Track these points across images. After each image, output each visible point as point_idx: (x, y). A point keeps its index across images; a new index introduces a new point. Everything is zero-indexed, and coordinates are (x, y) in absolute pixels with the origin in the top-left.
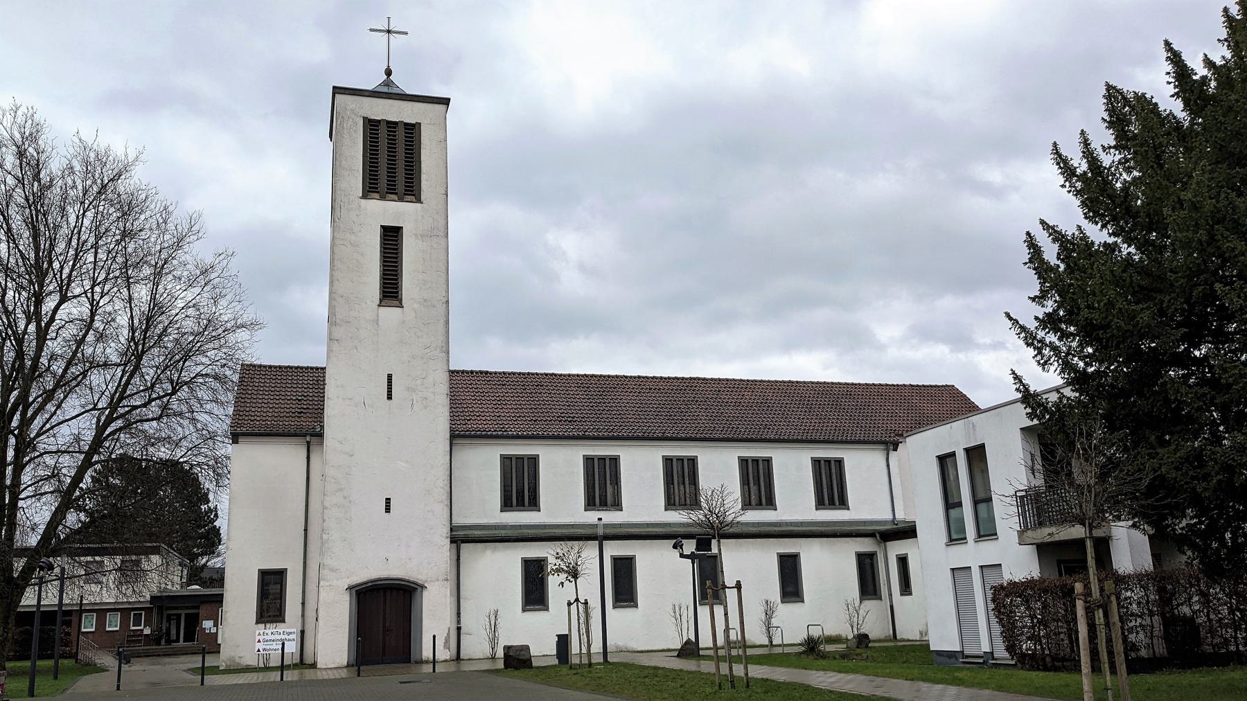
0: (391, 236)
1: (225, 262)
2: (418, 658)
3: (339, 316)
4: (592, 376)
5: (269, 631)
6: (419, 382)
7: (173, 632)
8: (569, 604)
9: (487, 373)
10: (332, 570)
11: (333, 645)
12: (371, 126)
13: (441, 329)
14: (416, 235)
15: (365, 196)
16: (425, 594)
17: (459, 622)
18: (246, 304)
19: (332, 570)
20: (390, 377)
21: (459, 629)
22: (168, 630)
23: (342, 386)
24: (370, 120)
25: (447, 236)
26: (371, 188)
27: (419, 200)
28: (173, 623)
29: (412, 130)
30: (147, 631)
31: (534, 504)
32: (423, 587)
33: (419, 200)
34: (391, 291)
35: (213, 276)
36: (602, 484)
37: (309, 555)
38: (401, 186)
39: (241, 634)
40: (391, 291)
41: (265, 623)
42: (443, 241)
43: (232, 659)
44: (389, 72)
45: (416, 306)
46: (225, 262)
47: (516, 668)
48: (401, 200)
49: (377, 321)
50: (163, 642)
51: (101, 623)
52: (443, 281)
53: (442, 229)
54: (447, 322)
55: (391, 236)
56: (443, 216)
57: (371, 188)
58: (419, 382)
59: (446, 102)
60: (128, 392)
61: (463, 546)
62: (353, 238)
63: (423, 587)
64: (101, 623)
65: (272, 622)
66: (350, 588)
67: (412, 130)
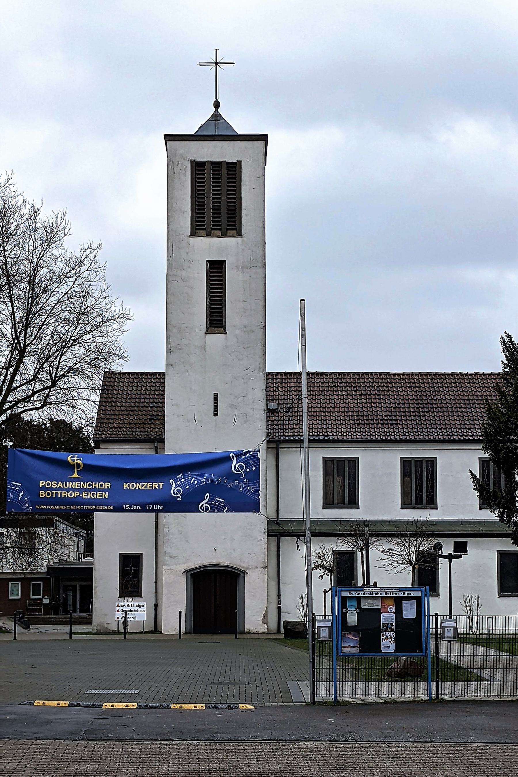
0: (216, 270)
1: (93, 255)
2: (241, 629)
3: (173, 344)
4: (427, 374)
5: (126, 604)
6: (240, 399)
7: (70, 601)
8: (325, 592)
9: (322, 374)
10: (172, 557)
11: (174, 615)
12: (198, 167)
13: (259, 352)
14: (237, 267)
15: (193, 234)
16: (247, 578)
17: (279, 602)
18: (112, 299)
19: (172, 557)
20: (216, 395)
21: (279, 608)
22: (65, 600)
23: (177, 405)
24: (197, 163)
25: (264, 267)
26: (199, 227)
27: (240, 235)
28: (70, 593)
29: (234, 168)
30: (46, 601)
31: (353, 502)
32: (245, 573)
33: (240, 235)
34: (216, 320)
35: (83, 269)
36: (419, 485)
37: (275, 503)
38: (224, 222)
39: (110, 607)
40: (216, 320)
41: (124, 597)
42: (260, 270)
43: (101, 625)
44: (217, 105)
45: (237, 332)
46: (93, 255)
47: (293, 638)
48: (224, 235)
49: (204, 348)
50: (61, 611)
51: (398, 611)
52: (261, 308)
53: (260, 259)
54: (264, 346)
55: (216, 270)
56: (261, 248)
57: (199, 227)
58: (240, 399)
59: (264, 138)
60: (14, 385)
61: (283, 539)
62: (184, 273)
63: (245, 573)
64: (398, 611)
65: (129, 596)
66: (186, 572)
67: (234, 168)
